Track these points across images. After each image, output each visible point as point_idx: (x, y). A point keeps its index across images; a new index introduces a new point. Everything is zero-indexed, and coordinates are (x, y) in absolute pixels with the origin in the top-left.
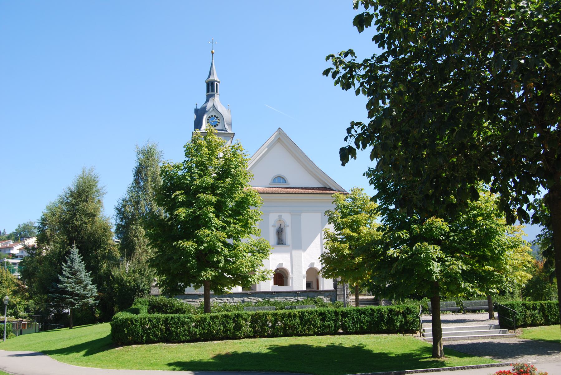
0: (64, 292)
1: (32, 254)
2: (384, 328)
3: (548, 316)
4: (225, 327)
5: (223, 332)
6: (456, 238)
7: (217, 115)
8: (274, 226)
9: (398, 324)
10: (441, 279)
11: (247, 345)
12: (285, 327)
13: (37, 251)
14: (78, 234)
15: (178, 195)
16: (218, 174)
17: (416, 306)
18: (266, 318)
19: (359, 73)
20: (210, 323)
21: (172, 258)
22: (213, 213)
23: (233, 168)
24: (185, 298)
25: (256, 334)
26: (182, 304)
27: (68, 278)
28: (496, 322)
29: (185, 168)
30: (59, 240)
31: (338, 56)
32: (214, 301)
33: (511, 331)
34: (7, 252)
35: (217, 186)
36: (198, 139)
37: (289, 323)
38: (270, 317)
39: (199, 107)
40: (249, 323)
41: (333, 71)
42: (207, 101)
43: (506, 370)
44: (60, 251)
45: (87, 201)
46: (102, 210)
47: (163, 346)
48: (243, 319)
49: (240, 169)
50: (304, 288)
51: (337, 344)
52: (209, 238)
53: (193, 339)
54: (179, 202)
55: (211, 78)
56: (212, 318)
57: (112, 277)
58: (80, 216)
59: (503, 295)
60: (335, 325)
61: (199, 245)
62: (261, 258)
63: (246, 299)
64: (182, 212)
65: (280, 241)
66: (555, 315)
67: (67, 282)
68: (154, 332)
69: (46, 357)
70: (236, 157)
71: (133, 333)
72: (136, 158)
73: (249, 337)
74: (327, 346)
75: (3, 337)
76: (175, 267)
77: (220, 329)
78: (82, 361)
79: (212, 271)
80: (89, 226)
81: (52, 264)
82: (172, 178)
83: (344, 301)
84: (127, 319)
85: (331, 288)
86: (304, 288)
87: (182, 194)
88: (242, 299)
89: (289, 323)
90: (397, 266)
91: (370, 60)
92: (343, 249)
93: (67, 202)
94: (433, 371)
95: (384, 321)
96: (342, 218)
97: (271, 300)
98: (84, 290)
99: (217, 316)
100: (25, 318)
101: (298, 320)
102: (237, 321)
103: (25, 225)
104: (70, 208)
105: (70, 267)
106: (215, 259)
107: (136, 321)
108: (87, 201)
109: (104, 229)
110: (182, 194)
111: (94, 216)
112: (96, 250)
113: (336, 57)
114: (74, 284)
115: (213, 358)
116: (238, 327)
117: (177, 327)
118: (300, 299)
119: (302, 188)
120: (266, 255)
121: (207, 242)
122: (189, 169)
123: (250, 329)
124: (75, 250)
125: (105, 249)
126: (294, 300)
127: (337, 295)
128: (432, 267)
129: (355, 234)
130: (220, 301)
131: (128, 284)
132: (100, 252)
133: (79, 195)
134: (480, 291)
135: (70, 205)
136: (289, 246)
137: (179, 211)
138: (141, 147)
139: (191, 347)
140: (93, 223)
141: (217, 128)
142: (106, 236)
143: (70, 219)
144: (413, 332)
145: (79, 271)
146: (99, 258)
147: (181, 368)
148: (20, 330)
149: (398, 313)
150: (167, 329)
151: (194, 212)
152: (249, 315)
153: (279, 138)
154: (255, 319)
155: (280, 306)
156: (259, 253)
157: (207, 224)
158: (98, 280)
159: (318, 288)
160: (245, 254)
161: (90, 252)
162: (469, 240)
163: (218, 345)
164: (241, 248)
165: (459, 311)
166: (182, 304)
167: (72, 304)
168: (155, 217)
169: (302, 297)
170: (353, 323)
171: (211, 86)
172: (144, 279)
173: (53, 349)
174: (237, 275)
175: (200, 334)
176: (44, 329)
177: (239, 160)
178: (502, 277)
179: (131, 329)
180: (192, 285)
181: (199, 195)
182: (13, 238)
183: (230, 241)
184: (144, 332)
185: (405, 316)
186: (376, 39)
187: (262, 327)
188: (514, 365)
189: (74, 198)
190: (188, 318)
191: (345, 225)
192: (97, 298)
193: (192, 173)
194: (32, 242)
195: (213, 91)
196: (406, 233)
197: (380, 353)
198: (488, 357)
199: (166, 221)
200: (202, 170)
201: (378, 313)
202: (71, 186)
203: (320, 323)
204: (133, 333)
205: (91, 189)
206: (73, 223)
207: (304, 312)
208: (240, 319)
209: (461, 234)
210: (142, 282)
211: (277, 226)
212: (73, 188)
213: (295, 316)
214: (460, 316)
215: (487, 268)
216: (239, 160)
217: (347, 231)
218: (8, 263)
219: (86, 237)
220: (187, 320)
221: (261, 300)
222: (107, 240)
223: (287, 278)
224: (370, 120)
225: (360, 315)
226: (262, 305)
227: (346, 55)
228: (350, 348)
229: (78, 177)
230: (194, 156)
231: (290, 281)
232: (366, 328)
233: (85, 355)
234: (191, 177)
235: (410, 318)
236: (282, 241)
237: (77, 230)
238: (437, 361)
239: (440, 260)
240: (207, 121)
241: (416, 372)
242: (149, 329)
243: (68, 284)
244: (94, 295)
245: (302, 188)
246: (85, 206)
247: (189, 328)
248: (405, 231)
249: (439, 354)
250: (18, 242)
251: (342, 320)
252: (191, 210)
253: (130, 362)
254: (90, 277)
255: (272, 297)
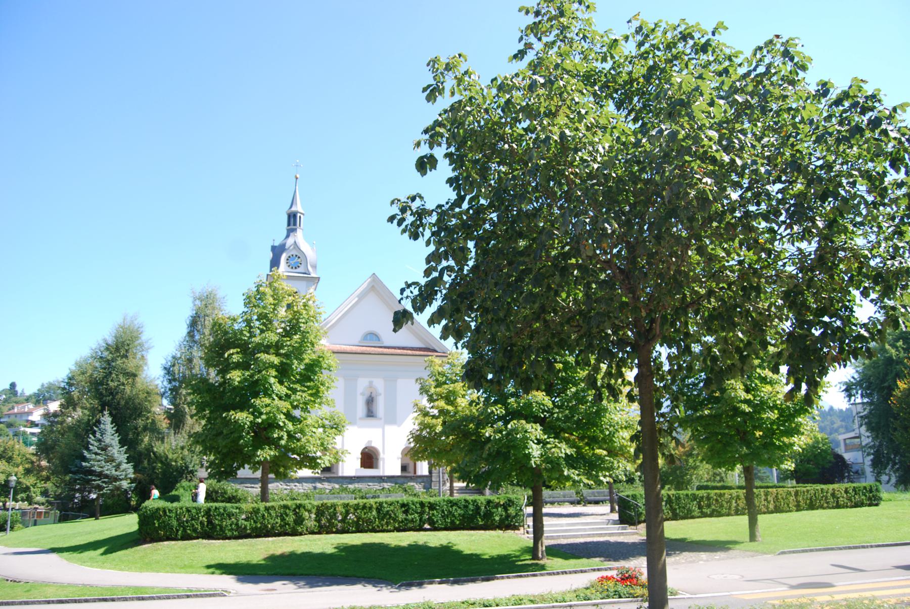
0: (91, 472)
1: (52, 422)
2: (481, 523)
3: (676, 509)
4: (283, 520)
5: (281, 526)
6: (560, 415)
7: (299, 255)
8: (362, 394)
9: (497, 518)
10: (541, 465)
11: (309, 543)
12: (358, 521)
13: (59, 419)
14: (113, 398)
15: (233, 354)
16: (284, 329)
17: (519, 497)
18: (335, 509)
19: (430, 221)
20: (263, 515)
21: (222, 432)
22: (275, 377)
23: (304, 323)
24: (242, 483)
25: (322, 530)
26: (236, 491)
27: (96, 454)
28: (616, 516)
29: (243, 321)
30: (88, 405)
31: (406, 200)
32: (276, 487)
33: (632, 527)
34: (24, 418)
35: (282, 344)
36: (261, 286)
37: (363, 516)
38: (340, 509)
39: (277, 244)
40: (313, 516)
41: (399, 217)
42: (288, 236)
43: (605, 575)
44: (89, 420)
45: (126, 357)
46: (145, 368)
47: (203, 544)
48: (306, 510)
49: (312, 324)
50: (397, 472)
51: (421, 543)
52: (268, 409)
53: (242, 534)
54: (233, 363)
55: (294, 209)
56: (267, 509)
57: (154, 453)
58: (117, 375)
59: (632, 483)
60: (421, 520)
61: (256, 417)
62: (333, 435)
63: (319, 485)
64: (236, 376)
65: (370, 414)
66: (684, 508)
67: (94, 460)
68: (193, 525)
69: (54, 556)
70: (306, 310)
71: (165, 526)
72: (191, 305)
73: (313, 533)
74: (410, 545)
75: (5, 530)
76: (224, 444)
77: (277, 523)
78: (97, 562)
79: (271, 449)
80: (128, 389)
81: (77, 435)
82: (226, 333)
83: (439, 489)
84: (158, 509)
85: (419, 473)
86: (397, 472)
87: (237, 353)
88: (314, 485)
89: (363, 516)
90: (489, 448)
91: (443, 206)
92: (434, 426)
93: (101, 358)
94: (528, 576)
95: (480, 514)
96: (436, 387)
97: (350, 486)
98: (116, 471)
99: (273, 507)
100: (43, 504)
101: (374, 513)
102: (298, 513)
103: (50, 384)
104: (105, 365)
105: (100, 441)
106: (275, 436)
107: (170, 511)
108: (126, 357)
109: (148, 393)
110: (237, 353)
111: (135, 375)
112: (135, 419)
113: (402, 201)
114: (103, 462)
115: (265, 559)
116: (299, 520)
117: (222, 519)
118: (387, 485)
119: (399, 348)
120: (340, 431)
121: (266, 414)
122: (248, 322)
123: (315, 523)
124: (107, 419)
125: (148, 418)
126: (378, 488)
127: (431, 481)
128: (530, 451)
129: (450, 408)
130: (285, 487)
131: (174, 463)
132: (140, 422)
133: (117, 349)
134: (588, 479)
135: (106, 361)
136: (381, 419)
137: (233, 374)
138: (198, 290)
139: (239, 545)
140: (133, 385)
141: (298, 270)
142: (149, 401)
143: (103, 378)
144: (515, 528)
145: (111, 446)
146: (140, 429)
147: (221, 571)
148: (31, 519)
149: (497, 505)
150: (210, 522)
151: (252, 376)
152: (313, 506)
153: (373, 286)
154: (320, 512)
155: (361, 494)
156: (332, 428)
157: (268, 393)
158: (136, 458)
159: (415, 473)
160: (314, 430)
161: (128, 422)
162: (575, 418)
163: (273, 542)
164: (309, 421)
165: (579, 503)
166: (236, 491)
167: (100, 488)
168: (204, 381)
169: (389, 484)
170: (442, 517)
171: (293, 219)
172: (195, 457)
173: (65, 545)
174: (303, 454)
175: (252, 529)
176: (64, 519)
177: (311, 313)
178: (613, 463)
179: (164, 522)
180: (247, 466)
181: (259, 355)
182: (34, 400)
183: (297, 413)
184: (179, 525)
185: (506, 510)
186: (450, 181)
187: (329, 521)
188: (617, 569)
189: (111, 353)
190: (237, 508)
191: (441, 396)
192: (133, 481)
193: (251, 327)
194: (54, 406)
195: (295, 224)
196: (501, 408)
197: (472, 555)
198: (597, 559)
199: (218, 386)
200: (264, 324)
201: (473, 505)
202: (107, 338)
203: (401, 516)
204: (165, 526)
205: (133, 342)
206: (107, 384)
207: (382, 503)
208: (302, 510)
209: (567, 412)
210: (191, 461)
211: (367, 394)
212: (111, 340)
213: (371, 508)
214: (578, 509)
215: (598, 451)
216: (311, 313)
217: (442, 403)
218: (24, 433)
219: (123, 403)
220: (235, 511)
221: (337, 486)
222: (151, 407)
223: (377, 459)
224: (426, 279)
225: (452, 506)
226: (339, 493)
227: (413, 199)
228: (435, 548)
229: (117, 326)
230: (255, 306)
231: (381, 463)
232: (458, 523)
233: (102, 554)
234: (250, 332)
235: (512, 511)
236: (372, 412)
237: (112, 393)
238: (537, 564)
239: (539, 442)
240: (286, 261)
241: (508, 577)
242: (187, 521)
243: (95, 462)
244: (129, 476)
245: (399, 348)
246: (124, 363)
247: (238, 521)
248: (499, 406)
249: (540, 555)
250: (40, 406)
251: (429, 513)
252: (247, 373)
253: (158, 563)
254: (126, 453)
255: (350, 483)
